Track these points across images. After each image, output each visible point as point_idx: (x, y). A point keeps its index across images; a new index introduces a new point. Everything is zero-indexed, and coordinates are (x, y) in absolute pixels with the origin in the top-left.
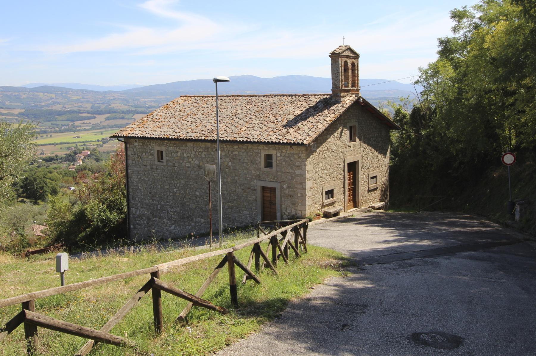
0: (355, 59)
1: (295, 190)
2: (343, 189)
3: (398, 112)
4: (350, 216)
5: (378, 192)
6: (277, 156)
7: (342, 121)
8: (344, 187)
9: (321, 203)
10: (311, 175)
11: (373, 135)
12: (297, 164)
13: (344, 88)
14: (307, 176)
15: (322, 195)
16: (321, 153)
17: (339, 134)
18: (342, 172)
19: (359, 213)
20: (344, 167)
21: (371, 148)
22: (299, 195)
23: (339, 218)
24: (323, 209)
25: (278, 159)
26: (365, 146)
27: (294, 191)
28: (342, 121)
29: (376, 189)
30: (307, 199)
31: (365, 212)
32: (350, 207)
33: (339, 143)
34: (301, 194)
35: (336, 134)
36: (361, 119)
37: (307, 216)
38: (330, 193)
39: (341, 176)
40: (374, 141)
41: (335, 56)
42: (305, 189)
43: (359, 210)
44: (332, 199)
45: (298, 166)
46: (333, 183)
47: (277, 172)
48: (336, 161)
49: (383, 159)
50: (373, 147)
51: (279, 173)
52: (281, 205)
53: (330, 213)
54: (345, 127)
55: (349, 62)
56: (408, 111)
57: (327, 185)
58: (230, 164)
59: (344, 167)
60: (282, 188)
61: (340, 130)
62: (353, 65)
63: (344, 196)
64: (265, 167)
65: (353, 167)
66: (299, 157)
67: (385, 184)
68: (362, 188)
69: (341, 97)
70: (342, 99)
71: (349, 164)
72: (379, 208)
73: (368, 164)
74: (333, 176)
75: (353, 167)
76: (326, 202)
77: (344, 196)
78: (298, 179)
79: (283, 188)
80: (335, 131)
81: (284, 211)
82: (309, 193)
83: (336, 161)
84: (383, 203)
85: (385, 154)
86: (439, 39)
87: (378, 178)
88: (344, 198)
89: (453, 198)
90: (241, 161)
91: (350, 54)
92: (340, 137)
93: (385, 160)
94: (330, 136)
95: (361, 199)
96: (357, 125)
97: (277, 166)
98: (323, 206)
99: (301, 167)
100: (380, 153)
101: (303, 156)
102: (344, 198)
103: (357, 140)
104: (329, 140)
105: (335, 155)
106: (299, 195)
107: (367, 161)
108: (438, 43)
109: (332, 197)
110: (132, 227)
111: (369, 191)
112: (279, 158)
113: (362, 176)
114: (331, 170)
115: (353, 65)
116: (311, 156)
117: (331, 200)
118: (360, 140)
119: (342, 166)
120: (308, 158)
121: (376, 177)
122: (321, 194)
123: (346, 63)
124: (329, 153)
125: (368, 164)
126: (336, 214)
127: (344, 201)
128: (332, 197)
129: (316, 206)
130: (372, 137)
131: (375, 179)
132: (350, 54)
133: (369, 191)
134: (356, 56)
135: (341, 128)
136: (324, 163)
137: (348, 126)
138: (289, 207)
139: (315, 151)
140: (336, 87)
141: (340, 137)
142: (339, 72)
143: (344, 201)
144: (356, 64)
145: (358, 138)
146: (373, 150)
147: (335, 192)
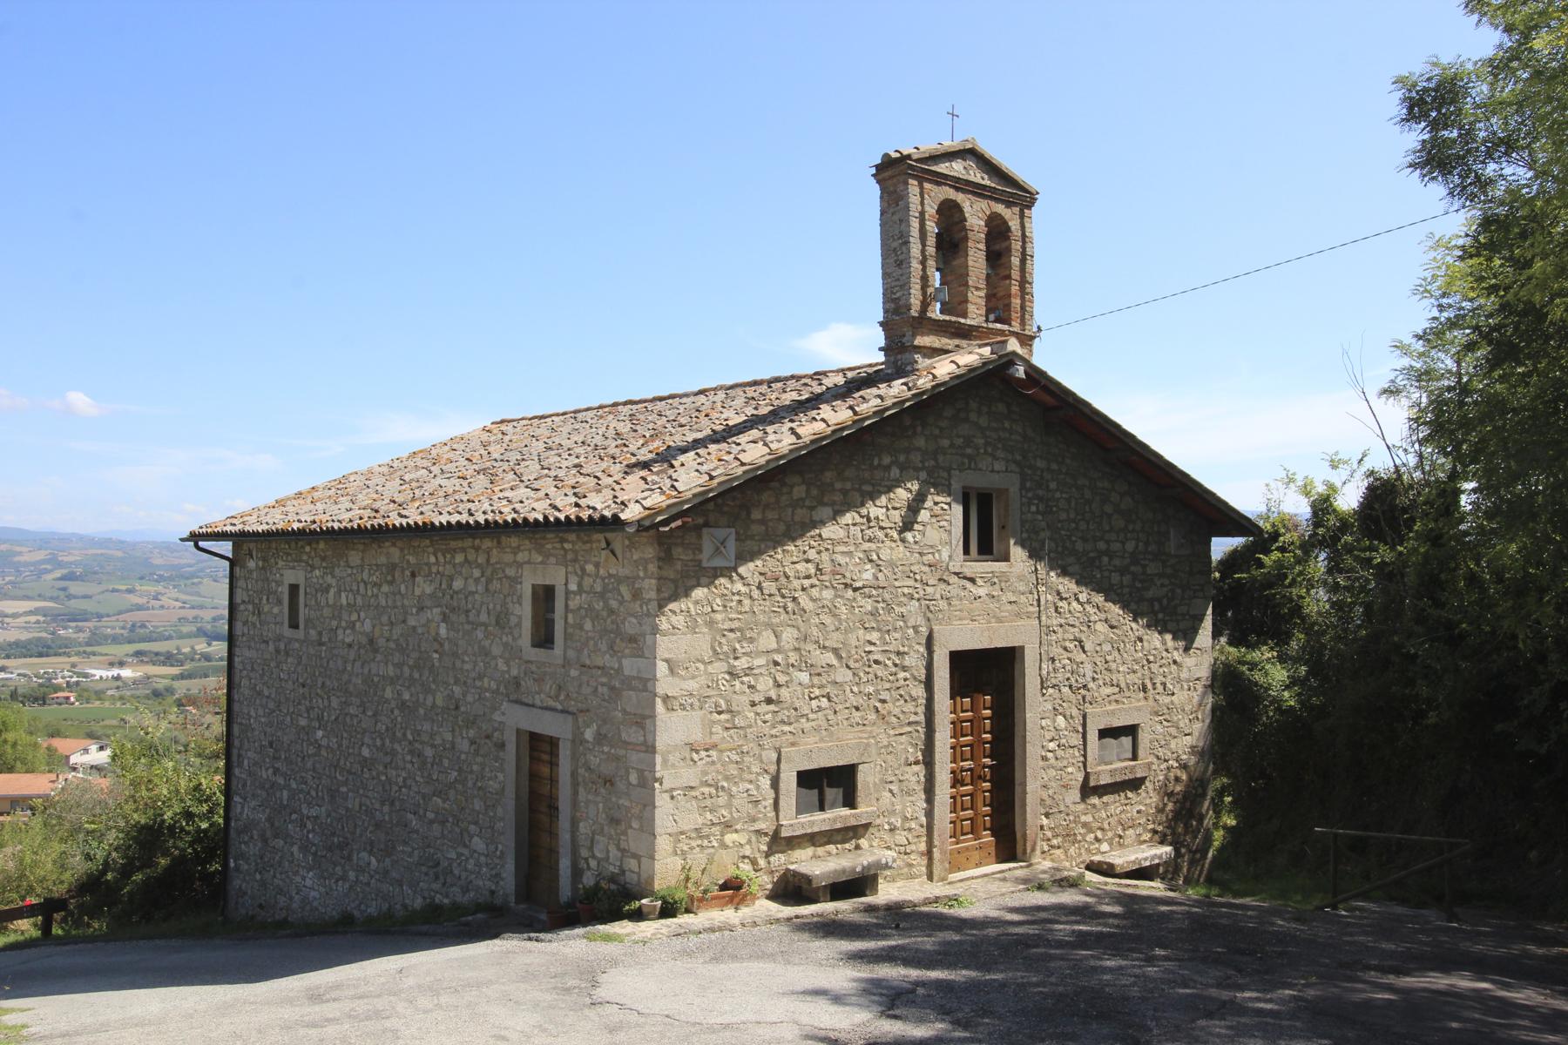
0: (1009, 205)
1: (622, 752)
2: (920, 769)
3: (1322, 507)
4: (937, 900)
5: (1146, 800)
6: (567, 592)
7: (916, 458)
8: (928, 761)
9: (766, 825)
10: (692, 685)
11: (1116, 546)
12: (631, 626)
13: (935, 312)
14: (665, 683)
15: (775, 783)
16: (770, 587)
17: (896, 516)
18: (919, 692)
19: (1008, 887)
20: (929, 667)
21: (1099, 599)
22: (633, 778)
23: (871, 909)
24: (779, 860)
25: (572, 604)
26: (1068, 585)
27: (618, 758)
28: (916, 458)
29: (1135, 784)
30: (662, 800)
31: (1040, 887)
32: (976, 855)
33: (891, 551)
34: (641, 772)
35: (873, 510)
36: (1040, 464)
37: (657, 887)
38: (831, 783)
39: (910, 707)
40: (1123, 571)
41: (894, 173)
42: (651, 749)
43: (1020, 873)
44: (846, 812)
45: (633, 639)
46: (851, 737)
47: (567, 663)
48: (874, 636)
49: (1176, 655)
50: (1111, 593)
51: (574, 673)
52: (574, 823)
53: (807, 879)
54: (936, 481)
55: (975, 213)
56: (1349, 499)
57: (810, 741)
58: (443, 631)
59: (929, 667)
60: (578, 740)
61: (902, 495)
62: (997, 232)
63: (930, 799)
64: (534, 646)
65: (988, 676)
66: (636, 595)
67: (1184, 767)
68: (1048, 770)
69: (918, 349)
70: (922, 362)
71: (957, 658)
72: (1141, 873)
73: (1088, 669)
74: (853, 700)
75: (988, 676)
76: (795, 822)
77: (930, 799)
78: (631, 699)
79: (583, 741)
80: (873, 496)
81: (584, 853)
82: (672, 772)
83: (874, 636)
84: (1169, 849)
85: (1186, 636)
86: (1400, 81)
87: (1144, 737)
88: (929, 814)
89: (1533, 855)
90: (472, 617)
91: (978, 176)
92: (907, 526)
93: (1189, 661)
94: (841, 512)
95: (1034, 819)
96: (1014, 490)
97: (567, 637)
98: (779, 842)
99: (640, 645)
100: (1160, 624)
101: (649, 586)
102: (929, 814)
103: (1017, 553)
104: (830, 531)
105: (868, 605)
106: (633, 778)
107: (1081, 657)
108: (1393, 105)
109: (850, 802)
110: (232, 865)
111: (1088, 790)
112: (574, 603)
113: (1044, 721)
114: (843, 675)
115: (997, 232)
116: (699, 593)
117: (838, 815)
118: (1034, 554)
119: (915, 661)
120: (674, 597)
121: (1131, 731)
122: (765, 782)
123: (949, 211)
124: (828, 594)
125: (1088, 669)
126: (854, 886)
127: (930, 828)
128: (850, 802)
129: (730, 838)
130: (1110, 554)
131: (1126, 741)
132: (978, 176)
133: (1088, 790)
134: (1023, 198)
135: (915, 486)
136: (789, 635)
137: (956, 486)
138: (602, 833)
139: (728, 571)
140: (896, 311)
141: (907, 526)
142: (907, 243)
143: (930, 828)
144: (1014, 224)
145: (1022, 544)
146: (1115, 610)
147: (865, 777)
